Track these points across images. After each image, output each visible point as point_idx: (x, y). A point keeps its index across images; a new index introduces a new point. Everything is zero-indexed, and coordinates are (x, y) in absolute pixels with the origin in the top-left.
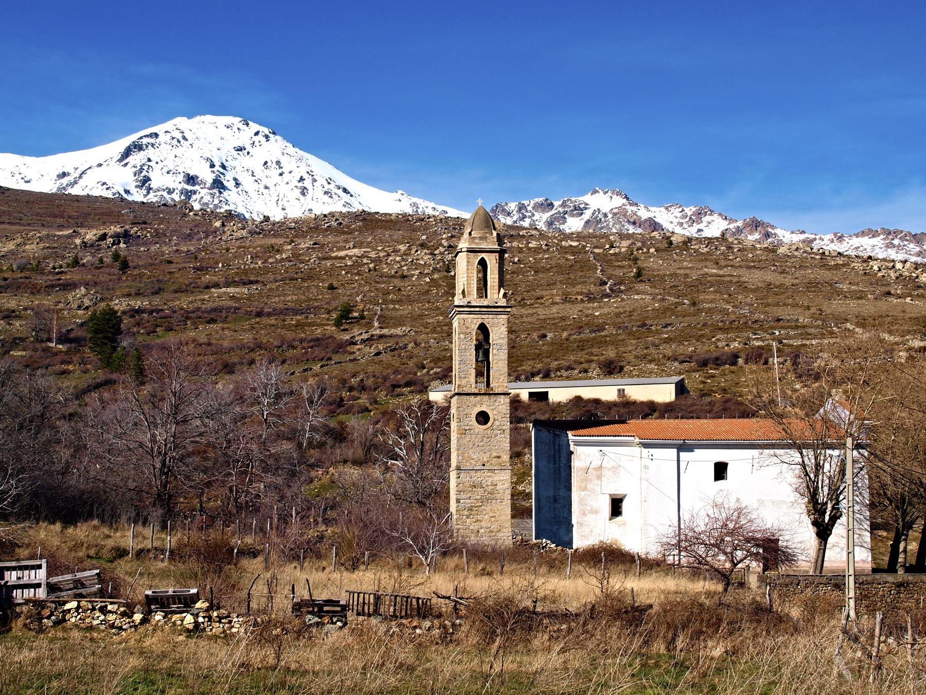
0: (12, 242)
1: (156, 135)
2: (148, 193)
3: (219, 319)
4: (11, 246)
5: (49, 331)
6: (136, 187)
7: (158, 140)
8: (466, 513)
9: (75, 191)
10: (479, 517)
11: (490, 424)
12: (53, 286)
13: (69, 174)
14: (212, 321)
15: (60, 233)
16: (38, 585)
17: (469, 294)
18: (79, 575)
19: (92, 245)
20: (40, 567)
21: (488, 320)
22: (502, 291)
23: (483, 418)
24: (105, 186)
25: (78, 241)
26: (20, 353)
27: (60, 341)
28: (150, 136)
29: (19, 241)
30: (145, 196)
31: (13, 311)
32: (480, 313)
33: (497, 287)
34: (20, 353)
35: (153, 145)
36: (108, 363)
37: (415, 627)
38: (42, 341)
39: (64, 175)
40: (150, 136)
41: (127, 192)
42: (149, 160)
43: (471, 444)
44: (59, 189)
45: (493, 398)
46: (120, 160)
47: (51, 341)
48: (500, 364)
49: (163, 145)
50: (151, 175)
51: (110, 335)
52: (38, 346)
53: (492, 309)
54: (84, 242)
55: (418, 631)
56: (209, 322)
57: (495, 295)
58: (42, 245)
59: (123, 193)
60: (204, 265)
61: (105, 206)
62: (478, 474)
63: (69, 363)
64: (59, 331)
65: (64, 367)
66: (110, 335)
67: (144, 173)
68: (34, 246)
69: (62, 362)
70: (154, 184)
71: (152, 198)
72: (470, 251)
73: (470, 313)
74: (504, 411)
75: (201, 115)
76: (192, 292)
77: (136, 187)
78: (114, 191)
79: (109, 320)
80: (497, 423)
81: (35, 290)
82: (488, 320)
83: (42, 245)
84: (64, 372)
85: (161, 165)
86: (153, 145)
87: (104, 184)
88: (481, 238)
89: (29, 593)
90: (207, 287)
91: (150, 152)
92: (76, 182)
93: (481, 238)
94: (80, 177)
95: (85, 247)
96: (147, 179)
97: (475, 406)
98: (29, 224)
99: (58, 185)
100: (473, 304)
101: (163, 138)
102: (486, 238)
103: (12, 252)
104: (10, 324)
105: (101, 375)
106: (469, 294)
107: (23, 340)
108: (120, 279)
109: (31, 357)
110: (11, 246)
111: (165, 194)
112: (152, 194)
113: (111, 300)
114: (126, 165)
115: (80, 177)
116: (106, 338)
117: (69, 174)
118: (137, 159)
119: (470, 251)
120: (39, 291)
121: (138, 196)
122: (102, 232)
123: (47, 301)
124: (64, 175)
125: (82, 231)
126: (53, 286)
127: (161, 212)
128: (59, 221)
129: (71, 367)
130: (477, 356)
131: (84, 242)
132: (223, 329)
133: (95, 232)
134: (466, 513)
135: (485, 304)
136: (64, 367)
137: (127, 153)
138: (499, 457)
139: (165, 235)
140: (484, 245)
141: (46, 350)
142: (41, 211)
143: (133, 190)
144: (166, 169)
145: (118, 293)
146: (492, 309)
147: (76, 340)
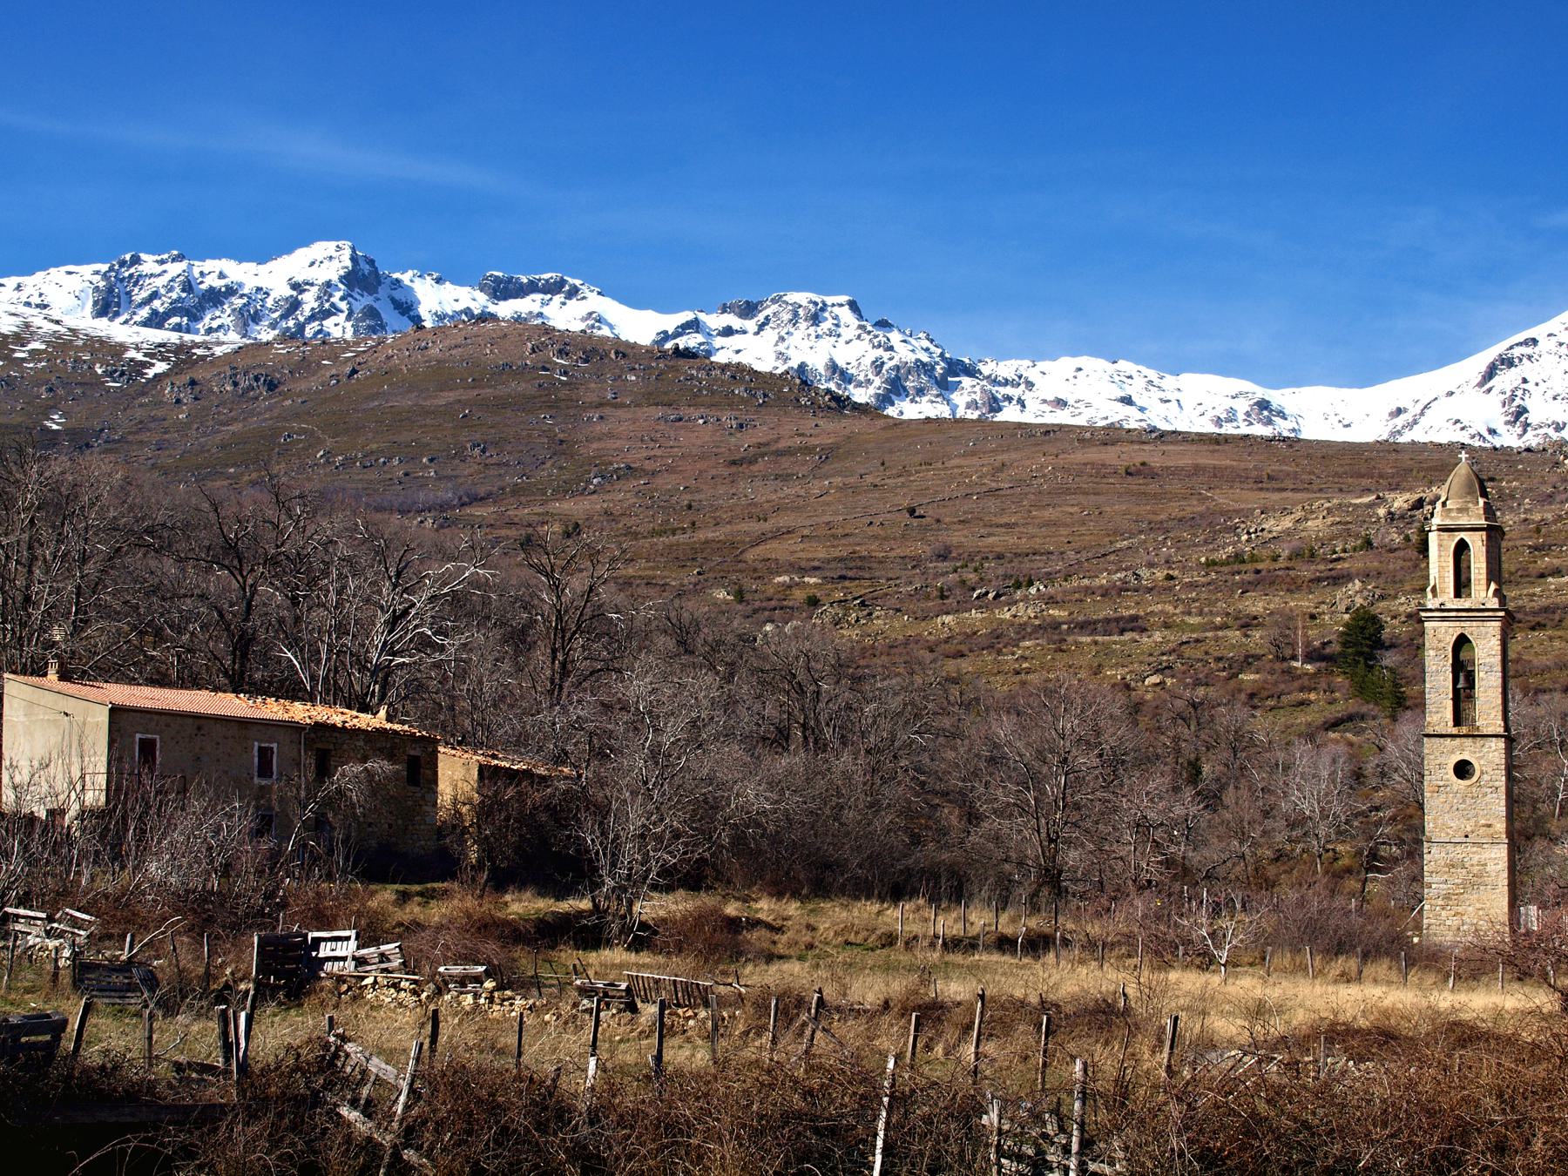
0: (1289, 518)
1: (1534, 341)
2: (1525, 431)
3: (1549, 624)
4: (1287, 523)
5: (1293, 645)
6: (1507, 423)
7: (1537, 349)
8: (1440, 902)
9: (1418, 435)
10: (1460, 909)
11: (1475, 779)
12: (1319, 580)
13: (1406, 410)
14: (1538, 626)
15: (1358, 501)
16: (344, 959)
17: (1443, 592)
18: (383, 948)
19: (1402, 517)
20: (348, 939)
21: (1470, 629)
22: (1493, 586)
23: (1463, 770)
24: (1459, 425)
25: (1382, 512)
26: (1252, 677)
27: (1309, 657)
28: (1525, 343)
29: (1299, 514)
30: (1520, 436)
31: (1255, 618)
32: (1458, 619)
33: (1484, 582)
34: (1252, 677)
35: (1530, 358)
36: (1361, 689)
37: (689, 1018)
38: (1284, 659)
39: (1399, 411)
40: (1525, 343)
41: (1492, 432)
42: (1525, 381)
43: (1447, 807)
44: (1392, 434)
45: (1479, 741)
46: (1481, 384)
47: (1294, 658)
48: (1490, 693)
49: (1545, 356)
50: (1528, 403)
51: (1366, 649)
52: (1278, 666)
53: (1478, 614)
54: (1390, 513)
55: (691, 1023)
56: (1533, 629)
57: (1482, 593)
58: (1330, 520)
59: (1485, 434)
60: (1550, 540)
61: (1436, 456)
62: (1459, 849)
63: (1310, 690)
64: (1308, 644)
65: (1302, 696)
66: (1366, 649)
67: (1518, 401)
68: (1319, 522)
69: (1302, 689)
70: (1533, 418)
71: (1532, 439)
72: (1443, 529)
73: (1444, 619)
74: (1497, 761)
75: (1091, 355)
76: (1518, 584)
77: (1507, 423)
78: (1473, 431)
79: (1363, 628)
80: (1486, 777)
81: (1294, 587)
82: (1470, 629)
83: (1330, 520)
84: (1302, 703)
85: (1543, 386)
86: (1530, 358)
87: (1457, 421)
88: (1460, 510)
89: (338, 965)
90: (1542, 576)
91: (1525, 369)
92: (1415, 422)
93: (1460, 510)
94: (1422, 414)
95: (1392, 519)
96: (1522, 411)
97: (1453, 752)
98: (1321, 490)
99: (1390, 428)
100: (1449, 606)
101: (1545, 344)
102: (1467, 509)
103: (1288, 532)
104: (1246, 636)
105: (1353, 706)
106: (1443, 592)
107: (1258, 658)
108: (1416, 566)
109: (1265, 681)
110: (1287, 523)
111: (1551, 431)
112: (1530, 433)
113: (1396, 597)
114: (1489, 390)
115: (1422, 414)
116: (1360, 654)
117: (1406, 410)
118: (1506, 380)
119: (1443, 529)
120: (1299, 588)
121: (1510, 438)
122: (1417, 496)
123: (1303, 603)
124: (1399, 411)
125: (1389, 496)
126: (1319, 580)
127: (1521, 461)
128: (1366, 482)
129: (1313, 696)
130: (1455, 681)
131: (1390, 513)
132: (1551, 639)
133: (1407, 496)
134: (1440, 902)
135: (1467, 606)
136: (1302, 696)
137: (1491, 373)
138: (1489, 826)
139: (1512, 497)
140: (1464, 521)
141: (1289, 672)
142: (1340, 470)
143: (1501, 429)
144: (1550, 394)
145: (1408, 587)
146: (1478, 614)
147: (1329, 659)
